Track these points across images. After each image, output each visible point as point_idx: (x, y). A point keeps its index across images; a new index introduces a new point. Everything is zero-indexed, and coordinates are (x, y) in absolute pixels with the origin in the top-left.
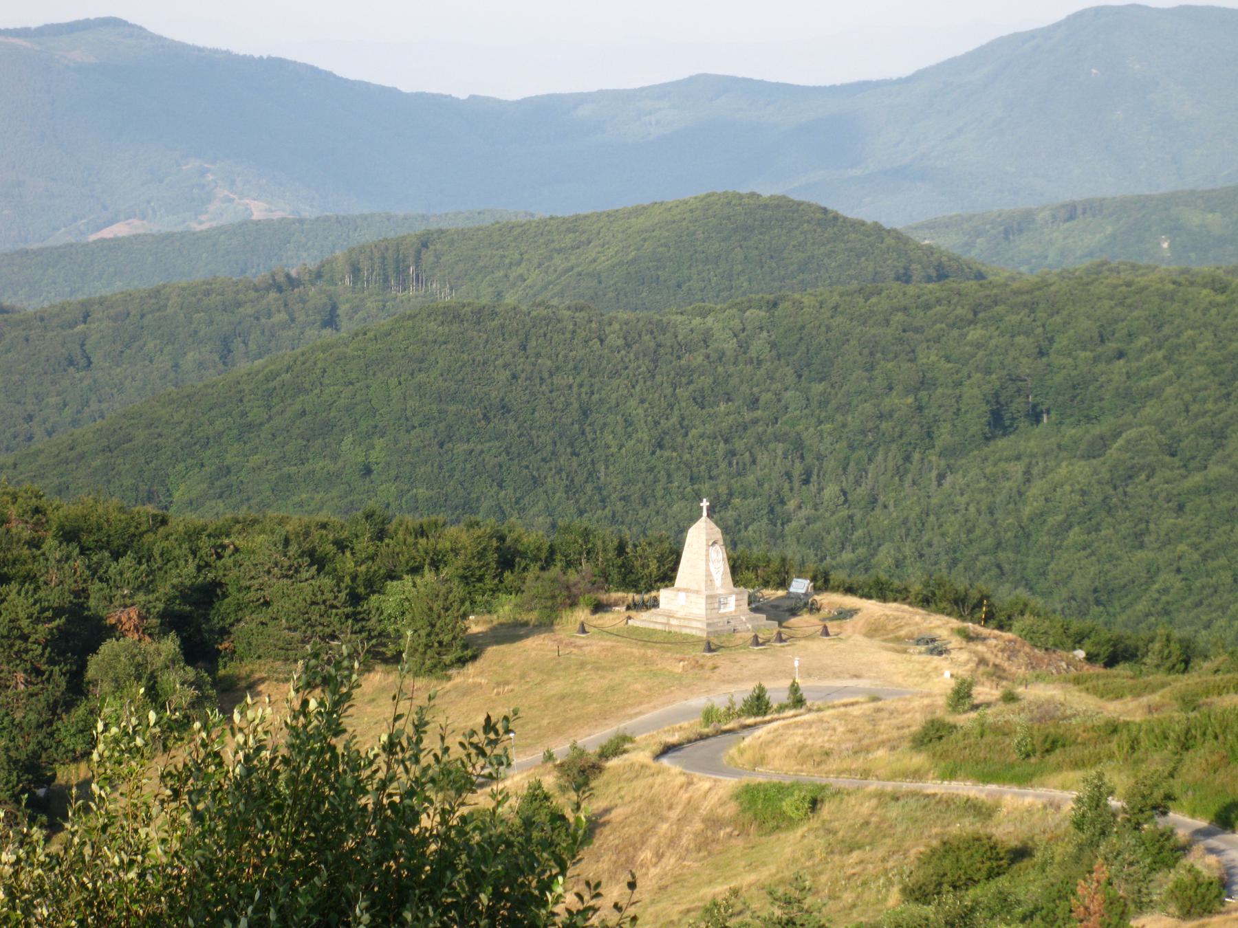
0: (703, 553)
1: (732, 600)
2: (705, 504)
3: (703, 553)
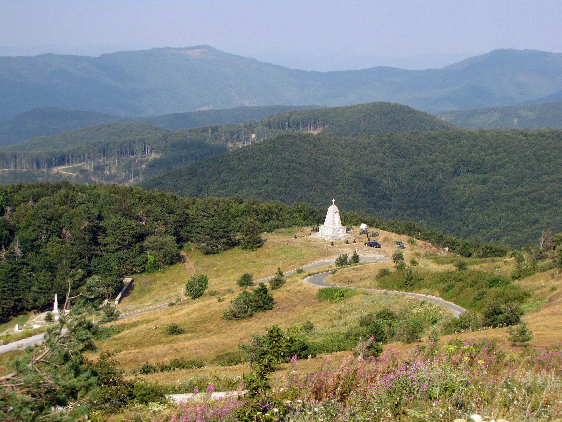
0: (333, 214)
1: (341, 230)
2: (334, 200)
3: (333, 214)
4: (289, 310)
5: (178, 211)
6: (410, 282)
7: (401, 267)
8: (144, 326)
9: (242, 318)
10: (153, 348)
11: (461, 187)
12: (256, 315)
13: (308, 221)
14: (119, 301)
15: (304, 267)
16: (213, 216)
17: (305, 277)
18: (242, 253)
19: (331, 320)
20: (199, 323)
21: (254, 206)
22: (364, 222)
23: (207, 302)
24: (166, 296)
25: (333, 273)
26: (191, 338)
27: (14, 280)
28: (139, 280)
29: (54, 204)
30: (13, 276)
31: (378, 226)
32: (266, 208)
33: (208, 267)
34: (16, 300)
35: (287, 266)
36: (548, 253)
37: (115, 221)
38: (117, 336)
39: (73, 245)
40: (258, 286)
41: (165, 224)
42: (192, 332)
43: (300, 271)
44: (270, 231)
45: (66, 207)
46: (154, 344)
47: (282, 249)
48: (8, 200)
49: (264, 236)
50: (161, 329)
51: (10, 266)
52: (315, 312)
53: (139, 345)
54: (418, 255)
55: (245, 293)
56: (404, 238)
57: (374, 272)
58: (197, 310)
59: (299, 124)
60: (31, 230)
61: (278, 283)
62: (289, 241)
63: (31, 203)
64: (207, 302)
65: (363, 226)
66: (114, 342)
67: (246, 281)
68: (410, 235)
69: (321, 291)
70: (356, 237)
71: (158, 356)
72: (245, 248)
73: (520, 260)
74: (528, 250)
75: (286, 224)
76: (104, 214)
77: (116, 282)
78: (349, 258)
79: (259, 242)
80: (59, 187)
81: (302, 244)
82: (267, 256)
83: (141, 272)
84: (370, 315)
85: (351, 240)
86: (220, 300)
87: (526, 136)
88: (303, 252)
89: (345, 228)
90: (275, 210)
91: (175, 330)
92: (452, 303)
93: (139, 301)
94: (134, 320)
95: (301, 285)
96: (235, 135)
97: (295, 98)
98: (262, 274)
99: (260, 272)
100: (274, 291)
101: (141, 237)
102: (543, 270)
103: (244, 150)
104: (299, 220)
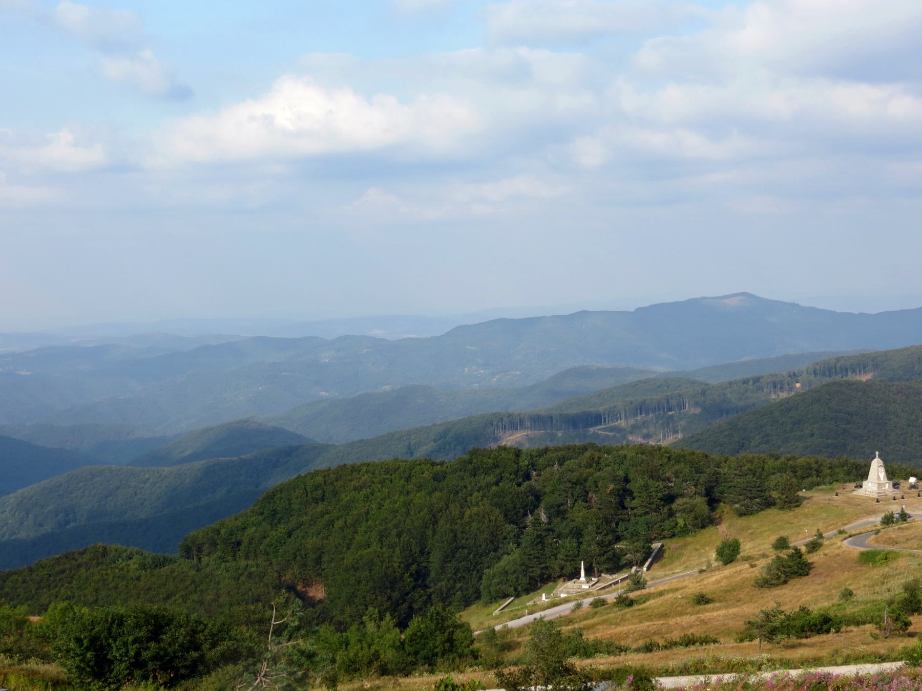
0: (877, 469)
3: (877, 469)
4: (827, 576)
8: (670, 595)
10: (679, 619)
12: (791, 582)
13: (852, 477)
14: (648, 568)
16: (746, 475)
17: (845, 539)
18: (778, 514)
19: (873, 586)
20: (728, 591)
21: (791, 463)
22: (912, 476)
23: (738, 568)
24: (697, 562)
25: (876, 534)
27: (539, 547)
28: (672, 544)
29: (580, 467)
30: (537, 544)
32: (805, 464)
34: (542, 568)
35: (827, 527)
37: (642, 482)
38: (641, 607)
39: (599, 509)
41: (696, 486)
42: (720, 601)
43: (841, 532)
46: (681, 614)
47: (822, 508)
48: (533, 465)
50: (687, 598)
51: (536, 533)
52: (855, 578)
53: (664, 615)
58: (726, 578)
59: (847, 370)
60: (556, 495)
61: (814, 546)
62: (829, 500)
63: (556, 466)
64: (738, 568)
65: (912, 480)
66: (637, 613)
69: (862, 554)
70: (905, 493)
71: (683, 628)
72: (782, 508)
76: (631, 476)
77: (644, 547)
79: (797, 501)
80: (585, 449)
81: (844, 502)
83: (671, 537)
85: (899, 496)
86: (752, 566)
88: (845, 511)
89: (891, 483)
90: (814, 466)
91: (702, 600)
93: (668, 567)
94: (661, 588)
95: (840, 547)
96: (777, 385)
97: (843, 345)
98: (801, 536)
99: (799, 534)
100: (811, 555)
101: (670, 499)
103: (787, 401)
104: (841, 476)
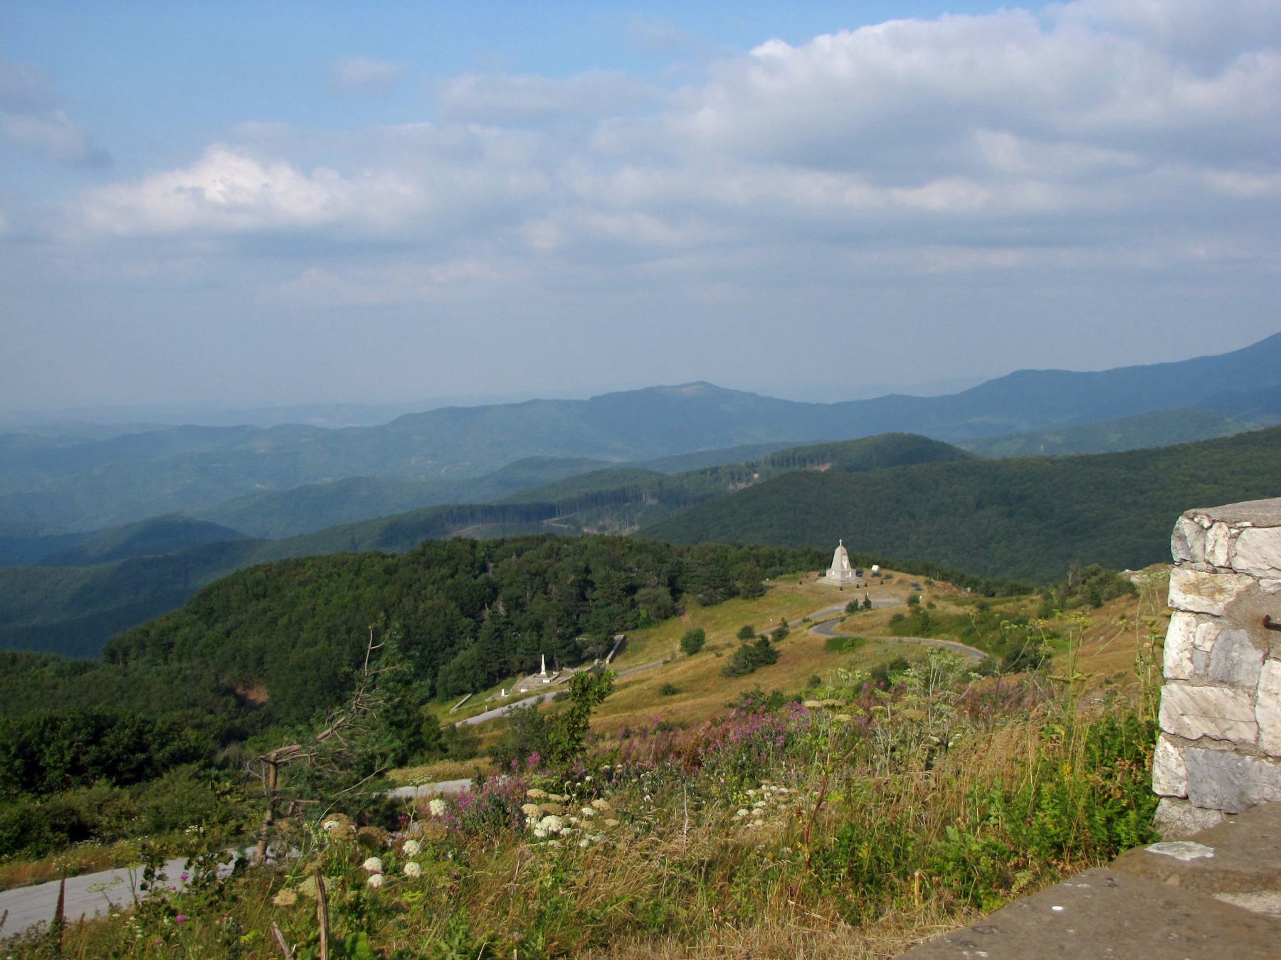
0: (841, 558)
3: (841, 558)
5: (670, 560)
6: (925, 625)
7: (917, 611)
8: (637, 686)
9: (743, 674)
10: (645, 711)
11: (985, 521)
12: (759, 670)
14: (611, 661)
15: (810, 616)
21: (754, 552)
23: (704, 658)
26: (685, 699)
27: (498, 640)
28: (634, 636)
31: (891, 568)
33: (706, 620)
36: (1078, 588)
40: (758, 639)
41: (658, 576)
43: (805, 621)
44: (773, 577)
45: (551, 561)
46: (647, 705)
49: (766, 582)
52: (822, 665)
54: (937, 597)
55: (745, 646)
56: (921, 579)
57: (886, 618)
61: (781, 634)
63: (514, 557)
64: (704, 658)
65: (875, 568)
67: (747, 633)
68: (927, 575)
69: (828, 641)
72: (746, 598)
73: (1048, 597)
74: (1056, 587)
75: (790, 569)
76: (591, 567)
78: (861, 603)
82: (770, 605)
84: (883, 666)
85: (862, 584)
86: (718, 656)
87: (1053, 462)
90: (777, 554)
91: (669, 690)
92: (973, 649)
96: (735, 476)
101: (632, 589)
102: (1074, 607)
